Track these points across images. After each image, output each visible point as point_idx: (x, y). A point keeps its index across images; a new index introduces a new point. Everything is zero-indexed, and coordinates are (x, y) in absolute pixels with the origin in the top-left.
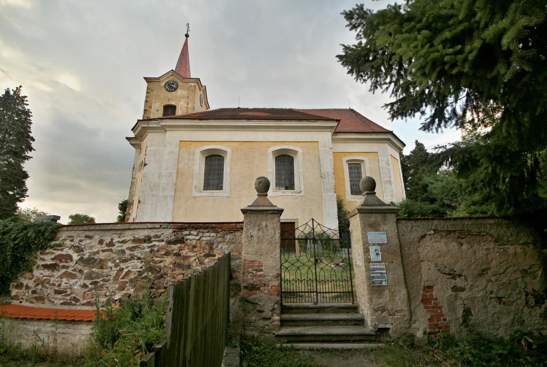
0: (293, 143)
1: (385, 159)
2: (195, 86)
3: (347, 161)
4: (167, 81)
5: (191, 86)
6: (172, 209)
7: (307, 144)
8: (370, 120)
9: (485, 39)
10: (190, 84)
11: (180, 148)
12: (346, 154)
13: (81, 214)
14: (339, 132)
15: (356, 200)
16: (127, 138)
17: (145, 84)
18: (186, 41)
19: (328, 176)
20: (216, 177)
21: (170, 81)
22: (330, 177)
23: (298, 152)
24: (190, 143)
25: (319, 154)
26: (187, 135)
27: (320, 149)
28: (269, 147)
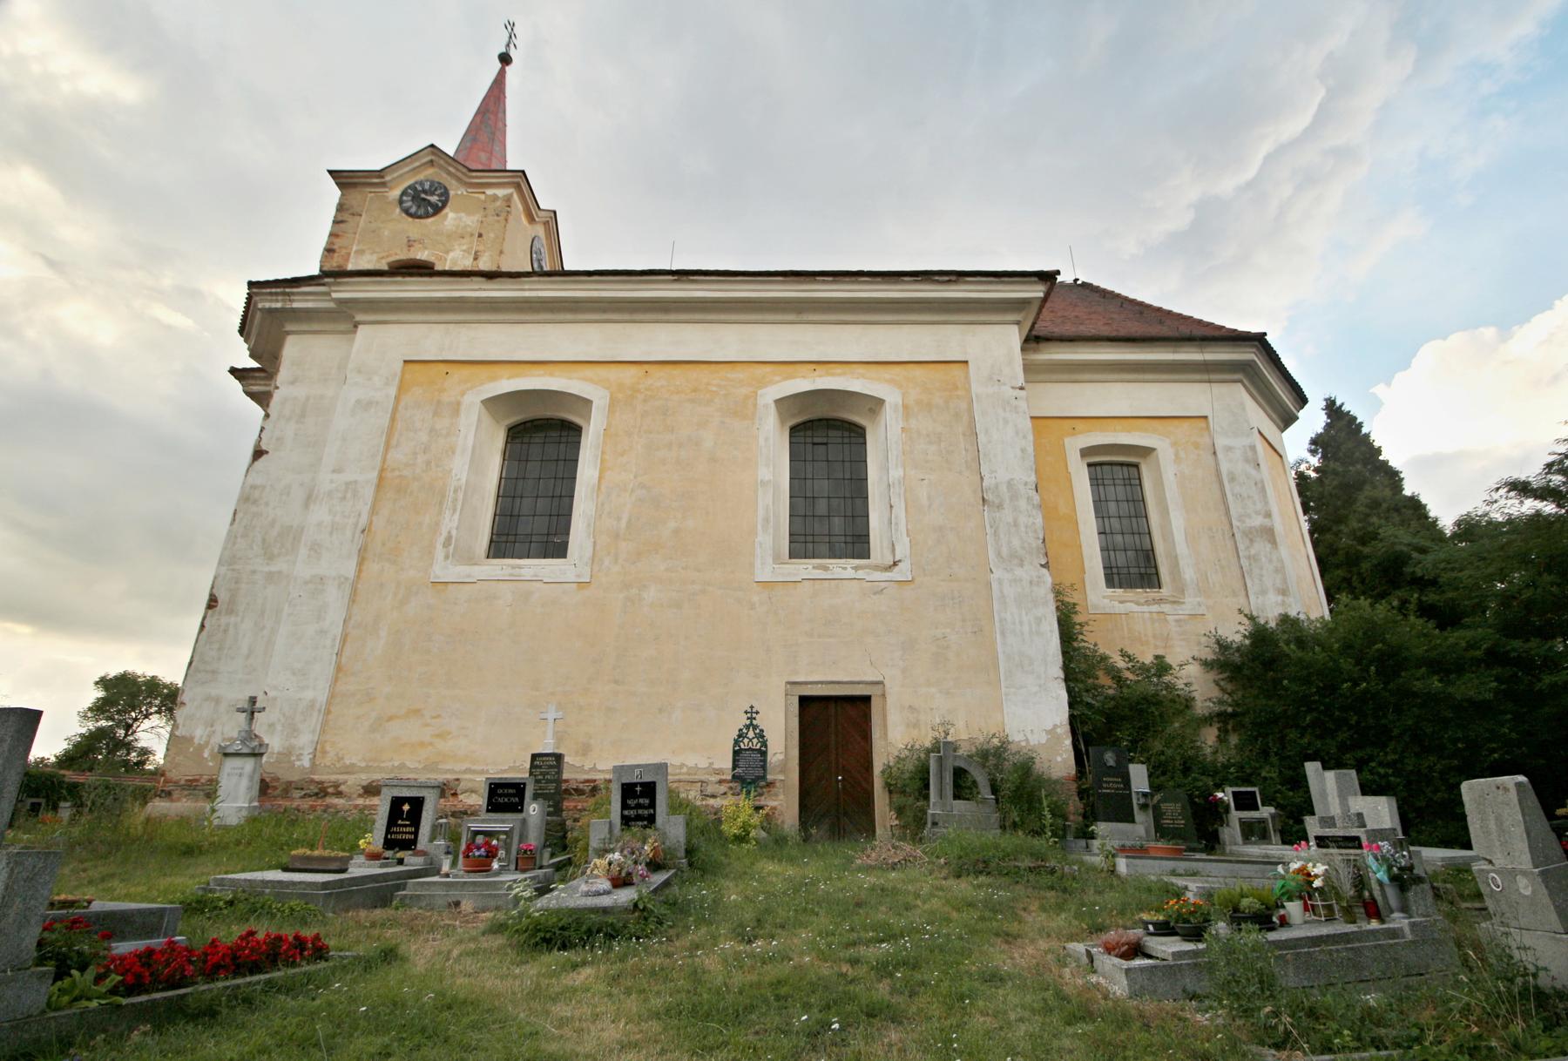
0: (861, 369)
1: (1239, 443)
2: (508, 199)
3: (1085, 452)
4: (411, 182)
5: (495, 198)
6: (338, 631)
7: (918, 372)
8: (1159, 309)
10: (489, 192)
11: (402, 389)
12: (1079, 425)
13: (139, 673)
14: (1048, 339)
15: (1135, 608)
16: (233, 371)
17: (334, 193)
19: (1014, 497)
21: (421, 183)
22: (1023, 504)
23: (881, 402)
25: (970, 410)
27: (976, 389)
28: (763, 383)
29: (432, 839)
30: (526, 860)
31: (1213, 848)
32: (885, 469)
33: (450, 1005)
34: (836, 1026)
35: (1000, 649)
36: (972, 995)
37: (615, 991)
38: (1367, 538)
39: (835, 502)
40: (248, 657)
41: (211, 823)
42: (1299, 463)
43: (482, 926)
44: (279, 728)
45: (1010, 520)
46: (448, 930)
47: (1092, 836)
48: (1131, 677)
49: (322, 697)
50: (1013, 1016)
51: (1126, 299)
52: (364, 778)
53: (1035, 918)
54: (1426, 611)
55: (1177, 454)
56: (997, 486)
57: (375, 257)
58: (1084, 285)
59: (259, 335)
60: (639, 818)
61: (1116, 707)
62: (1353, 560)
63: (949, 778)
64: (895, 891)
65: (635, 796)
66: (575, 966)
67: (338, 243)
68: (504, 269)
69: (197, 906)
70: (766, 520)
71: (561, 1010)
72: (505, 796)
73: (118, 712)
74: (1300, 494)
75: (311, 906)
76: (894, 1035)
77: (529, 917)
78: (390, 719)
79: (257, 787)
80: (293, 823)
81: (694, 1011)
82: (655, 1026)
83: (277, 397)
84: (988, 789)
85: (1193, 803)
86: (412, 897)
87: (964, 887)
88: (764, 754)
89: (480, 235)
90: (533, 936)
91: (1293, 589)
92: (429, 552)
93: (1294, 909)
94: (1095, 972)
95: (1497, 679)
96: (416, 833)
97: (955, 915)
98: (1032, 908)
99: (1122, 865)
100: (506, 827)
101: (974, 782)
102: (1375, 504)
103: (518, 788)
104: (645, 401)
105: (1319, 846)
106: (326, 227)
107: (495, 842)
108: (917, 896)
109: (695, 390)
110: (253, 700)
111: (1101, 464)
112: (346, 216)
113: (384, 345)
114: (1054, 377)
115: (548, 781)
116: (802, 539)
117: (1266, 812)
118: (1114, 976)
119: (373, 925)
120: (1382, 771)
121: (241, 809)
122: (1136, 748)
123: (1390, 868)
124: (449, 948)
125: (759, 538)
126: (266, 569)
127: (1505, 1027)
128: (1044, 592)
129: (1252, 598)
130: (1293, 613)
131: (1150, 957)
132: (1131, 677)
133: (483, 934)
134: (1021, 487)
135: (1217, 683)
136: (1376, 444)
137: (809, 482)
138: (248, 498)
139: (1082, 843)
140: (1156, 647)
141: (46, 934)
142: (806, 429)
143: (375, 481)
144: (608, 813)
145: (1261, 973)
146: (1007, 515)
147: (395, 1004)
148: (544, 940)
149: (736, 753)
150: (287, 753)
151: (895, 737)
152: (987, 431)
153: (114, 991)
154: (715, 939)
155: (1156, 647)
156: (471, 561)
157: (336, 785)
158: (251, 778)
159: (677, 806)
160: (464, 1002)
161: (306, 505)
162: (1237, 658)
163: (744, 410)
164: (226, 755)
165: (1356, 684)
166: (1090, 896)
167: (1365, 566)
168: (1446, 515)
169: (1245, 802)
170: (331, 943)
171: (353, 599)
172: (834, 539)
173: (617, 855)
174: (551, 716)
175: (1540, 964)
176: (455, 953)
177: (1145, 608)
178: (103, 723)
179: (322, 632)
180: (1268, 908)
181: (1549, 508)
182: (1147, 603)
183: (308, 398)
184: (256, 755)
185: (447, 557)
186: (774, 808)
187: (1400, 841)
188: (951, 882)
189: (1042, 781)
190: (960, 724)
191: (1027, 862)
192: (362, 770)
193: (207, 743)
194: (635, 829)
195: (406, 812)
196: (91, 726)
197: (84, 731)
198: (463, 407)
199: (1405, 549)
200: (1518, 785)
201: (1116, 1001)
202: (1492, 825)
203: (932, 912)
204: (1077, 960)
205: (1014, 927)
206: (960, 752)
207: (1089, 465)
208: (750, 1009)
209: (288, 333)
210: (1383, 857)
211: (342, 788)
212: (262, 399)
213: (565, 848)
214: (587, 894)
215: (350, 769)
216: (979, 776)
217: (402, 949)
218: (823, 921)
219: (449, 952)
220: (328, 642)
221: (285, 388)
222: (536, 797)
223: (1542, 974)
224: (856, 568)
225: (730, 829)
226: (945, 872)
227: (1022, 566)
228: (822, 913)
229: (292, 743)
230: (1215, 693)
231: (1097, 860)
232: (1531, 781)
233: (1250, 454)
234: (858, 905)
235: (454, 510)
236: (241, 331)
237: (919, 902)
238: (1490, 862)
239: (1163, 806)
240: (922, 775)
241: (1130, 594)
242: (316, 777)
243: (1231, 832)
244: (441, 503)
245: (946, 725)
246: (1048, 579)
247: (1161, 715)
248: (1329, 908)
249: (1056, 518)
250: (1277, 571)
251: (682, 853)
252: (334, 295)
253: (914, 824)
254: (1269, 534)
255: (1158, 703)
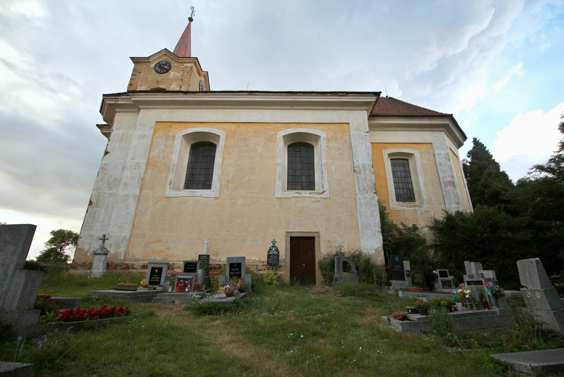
0: (312, 126)
1: (443, 152)
2: (192, 67)
3: (390, 155)
5: (187, 67)
6: (133, 213)
7: (332, 126)
10: (185, 65)
11: (155, 131)
12: (388, 146)
16: (98, 125)
17: (132, 65)
18: (189, 24)
19: (365, 169)
21: (162, 62)
22: (368, 172)
23: (319, 137)
24: (169, 124)
26: (166, 114)
27: (352, 132)
28: (279, 130)
29: (165, 282)
30: (197, 288)
31: (432, 290)
32: (320, 159)
33: (173, 328)
34: (302, 336)
35: (359, 221)
37: (228, 327)
38: (486, 186)
40: (103, 222)
41: (90, 276)
42: (464, 160)
43: (182, 308)
46: (171, 309)
48: (405, 232)
50: (362, 337)
51: (404, 103)
52: (142, 263)
53: (370, 310)
54: (507, 211)
55: (421, 156)
56: (359, 166)
57: (146, 87)
58: (390, 98)
59: (106, 113)
60: (235, 275)
62: (482, 194)
63: (341, 265)
65: (234, 268)
66: (214, 320)
67: (133, 82)
68: (190, 90)
69: (87, 300)
70: (280, 177)
71: (210, 331)
72: (190, 267)
73: (58, 243)
74: (464, 171)
75: (125, 301)
76: (322, 341)
78: (151, 243)
79: (106, 265)
80: (118, 277)
82: (241, 337)
83: (113, 133)
85: (425, 275)
87: (346, 300)
88: (278, 256)
89: (182, 80)
90: (199, 310)
91: (461, 201)
92: (164, 187)
93: (459, 305)
94: (390, 325)
95: (532, 234)
96: (160, 279)
97: (343, 307)
99: (400, 293)
100: (190, 277)
101: (350, 266)
102: (490, 174)
104: (238, 136)
105: (468, 284)
106: (129, 76)
108: (330, 302)
109: (255, 132)
110: (104, 236)
111: (395, 159)
112: (136, 73)
113: (150, 116)
114: (379, 129)
115: (204, 264)
117: (450, 278)
118: (397, 325)
119: (146, 307)
120: (491, 264)
122: (406, 256)
123: (492, 291)
124: (171, 313)
125: (277, 183)
126: (109, 192)
127: (531, 341)
129: (447, 205)
130: (461, 211)
131: (409, 320)
132: (405, 232)
135: (434, 234)
136: (491, 154)
137: (294, 164)
138: (103, 168)
139: (387, 287)
140: (413, 222)
141: (37, 301)
142: (293, 146)
144: (225, 274)
145: (447, 323)
146: (362, 176)
150: (116, 254)
151: (323, 250)
152: (355, 147)
153: (60, 320)
154: (261, 313)
156: (178, 189)
157: (132, 265)
158: (104, 262)
159: (248, 272)
160: (177, 328)
161: (123, 171)
162: (441, 226)
163: (272, 139)
164: (95, 254)
165: (482, 234)
167: (486, 196)
168: (514, 178)
169: (443, 274)
171: (138, 203)
173: (228, 286)
174: (206, 242)
175: (543, 321)
176: (174, 315)
177: (410, 209)
178: (53, 247)
179: (128, 213)
180: (450, 304)
181: (550, 176)
182: (410, 207)
183: (123, 134)
184: (105, 254)
185: (170, 188)
186: (282, 274)
187: (496, 282)
189: (373, 266)
190: (345, 247)
191: (368, 292)
192: (141, 260)
193: (89, 251)
194: (234, 278)
195: (156, 272)
196: (49, 247)
197: (46, 249)
198: (176, 138)
199: (500, 190)
200: (537, 261)
201: (398, 333)
202: (528, 275)
204: (385, 322)
205: (363, 312)
206: (345, 256)
207: (391, 159)
208: (273, 332)
209: (117, 112)
210: (490, 287)
211: (134, 266)
212: (107, 135)
213: (210, 286)
214: (218, 298)
215: (137, 260)
219: (172, 315)
220: (130, 217)
221: (116, 131)
222: (200, 268)
223: (544, 325)
224: (310, 193)
226: (340, 295)
227: (367, 193)
229: (118, 250)
230: (434, 238)
231: (392, 292)
232: (541, 260)
233: (446, 156)
234: (310, 304)
236: (100, 112)
238: (527, 287)
239: (415, 275)
240: (332, 263)
241: (404, 204)
242: (126, 262)
243: (438, 285)
244: (168, 170)
248: (471, 305)
249: (379, 179)
250: (455, 196)
251: (250, 287)
252: (132, 99)
253: (329, 280)
254: (453, 183)
255: (414, 241)
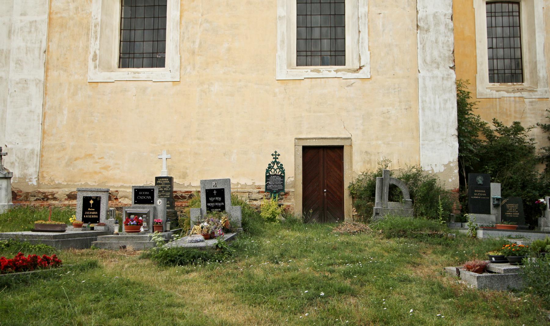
6: (40, 111)
9: (468, 98)
19: (437, 24)
20: (148, 35)
22: (442, 28)
29: (107, 218)
30: (158, 227)
35: (421, 119)
36: (394, 287)
37: (209, 282)
39: (324, 30)
43: (139, 256)
44: (17, 164)
45: (434, 40)
47: (466, 221)
49: (38, 148)
50: (414, 295)
52: (67, 191)
53: (430, 257)
60: (216, 207)
61: (487, 153)
63: (386, 190)
64: (354, 244)
65: (213, 196)
66: (188, 272)
70: (283, 42)
72: (143, 195)
77: (162, 250)
79: (10, 196)
80: (33, 212)
81: (250, 290)
82: (230, 295)
84: (408, 196)
85: (525, 204)
86: (100, 244)
87: (392, 243)
88: (283, 177)
90: (165, 259)
94: (460, 279)
96: (99, 215)
97: (386, 254)
98: (428, 252)
99: (480, 234)
101: (401, 192)
103: (150, 191)
107: (140, 218)
108: (366, 246)
115: (166, 191)
116: (304, 53)
118: (470, 280)
121: (4, 206)
122: (496, 176)
124: (122, 262)
125: (279, 53)
128: (451, 85)
131: (492, 272)
133: (140, 259)
134: (442, 17)
137: (309, 17)
139: (460, 224)
140: (515, 117)
143: (47, 20)
144: (199, 206)
146: (432, 36)
147: (99, 283)
148: (171, 261)
149: (268, 177)
150: (24, 178)
151: (357, 168)
154: (259, 262)
155: (515, 117)
156: (109, 69)
157: (53, 194)
158: (7, 190)
159: (235, 203)
160: (134, 283)
161: (9, 37)
166: (461, 247)
170: (63, 261)
171: (45, 93)
172: (323, 53)
173: (206, 224)
174: (164, 156)
176: (126, 266)
177: (512, 95)
182: (514, 91)
185: (95, 67)
186: (289, 206)
188: (385, 241)
189: (439, 191)
190: (395, 161)
191: (428, 232)
195: (91, 205)
203: (374, 253)
204: (451, 274)
205: (418, 260)
206: (394, 176)
208: (279, 288)
211: (56, 196)
214: (191, 242)
215: (58, 186)
216: (404, 190)
217: (99, 263)
218: (316, 254)
219: (123, 266)
224: (337, 71)
225: (265, 215)
227: (438, 68)
228: (315, 252)
234: (335, 249)
235: (96, 38)
237: (367, 248)
240: (371, 188)
241: (504, 86)
242: (41, 190)
245: (387, 161)
246: (454, 76)
247: (513, 157)
251: (240, 225)
253: (366, 213)
